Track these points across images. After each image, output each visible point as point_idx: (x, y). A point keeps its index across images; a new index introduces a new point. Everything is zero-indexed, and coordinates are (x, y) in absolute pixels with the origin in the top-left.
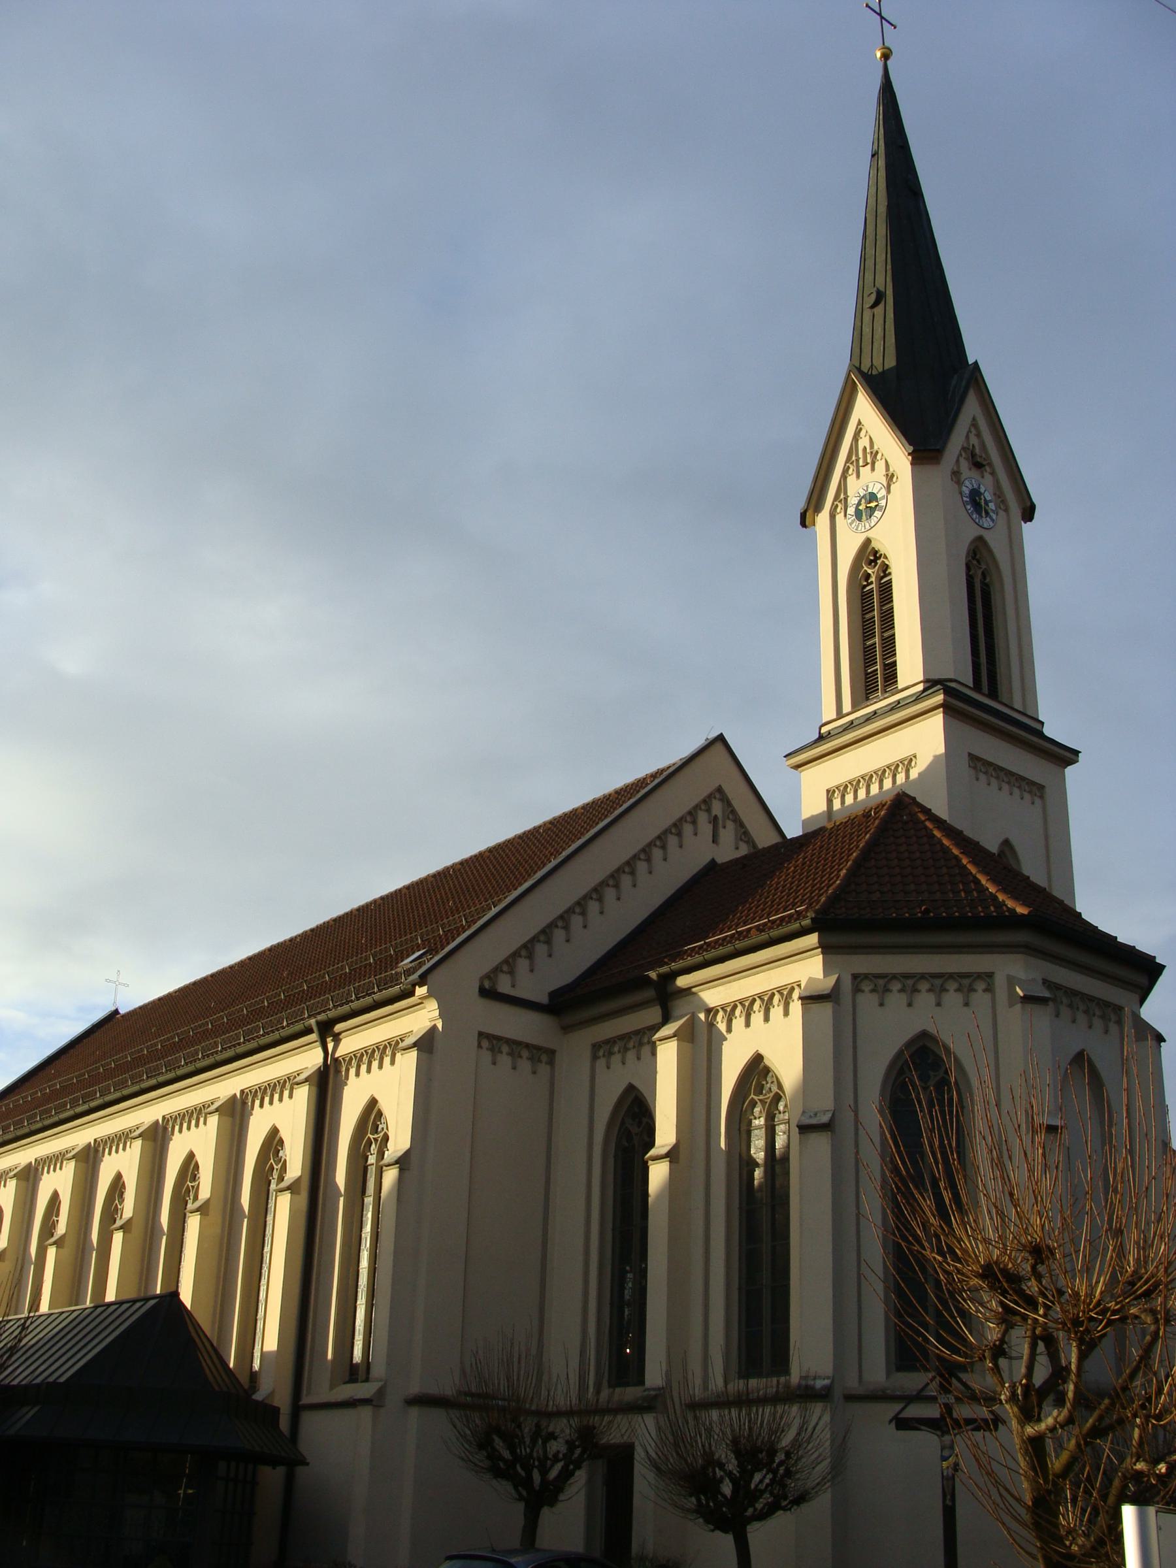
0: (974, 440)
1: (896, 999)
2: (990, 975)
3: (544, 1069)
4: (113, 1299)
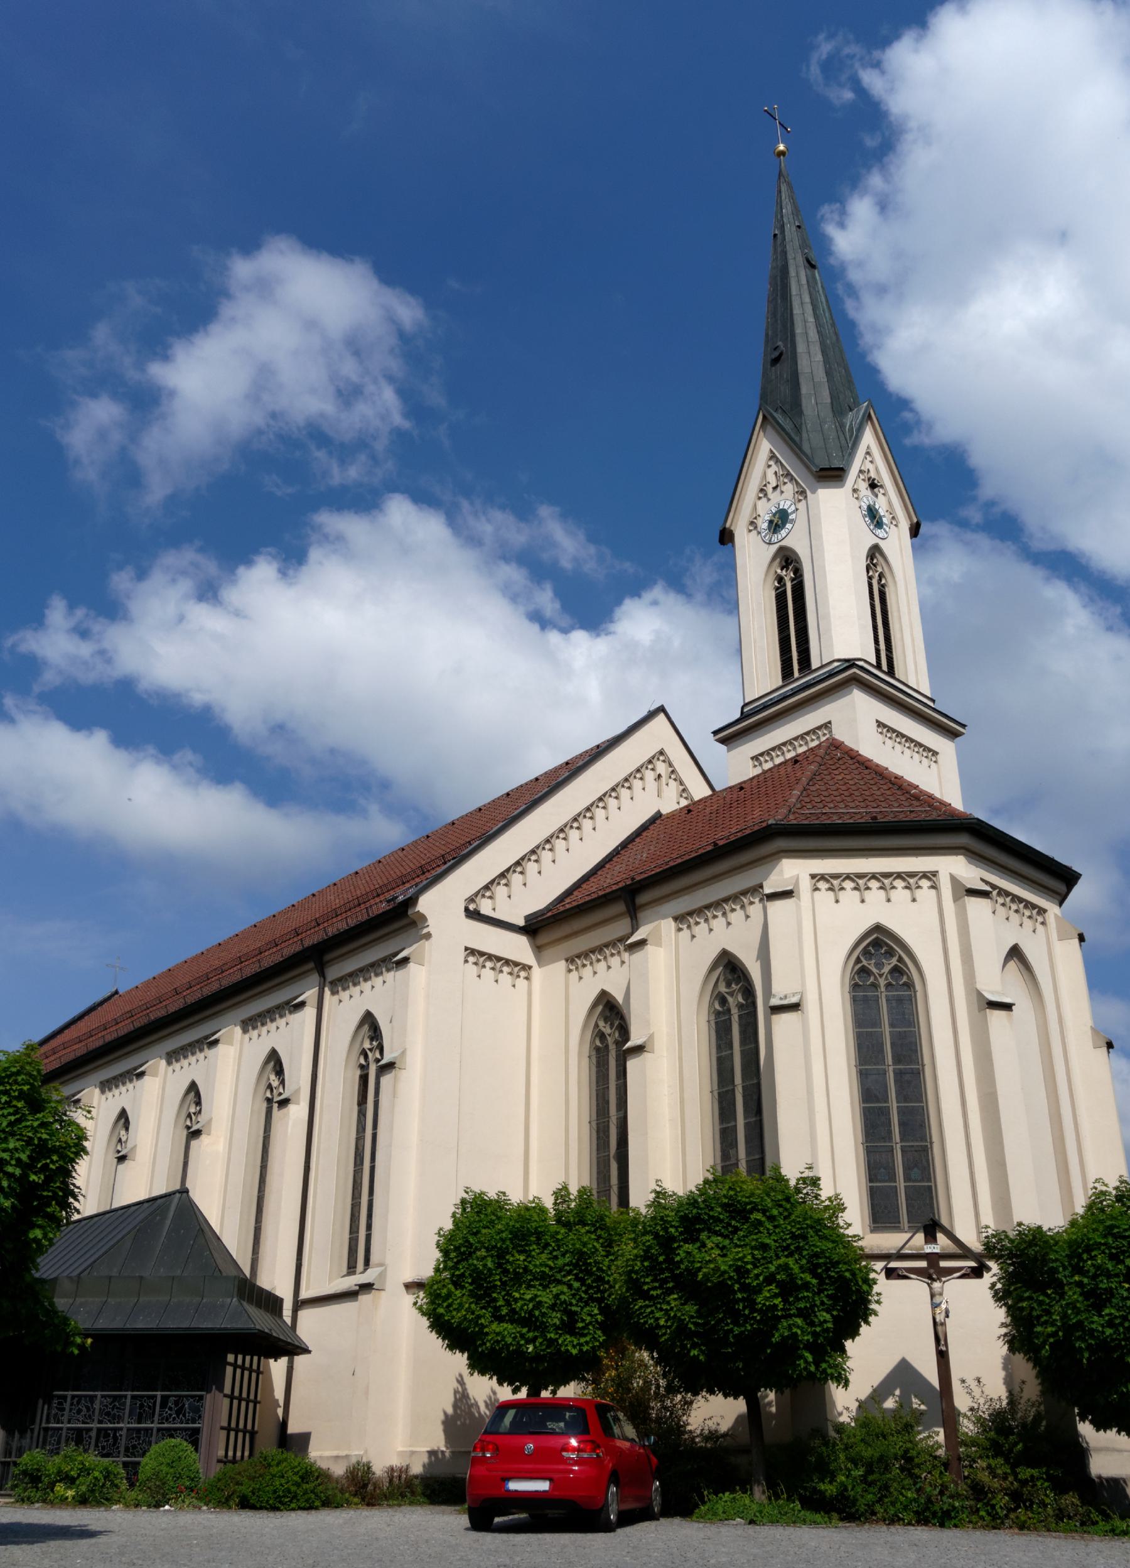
0: (871, 467)
2: (935, 874)
3: (521, 983)
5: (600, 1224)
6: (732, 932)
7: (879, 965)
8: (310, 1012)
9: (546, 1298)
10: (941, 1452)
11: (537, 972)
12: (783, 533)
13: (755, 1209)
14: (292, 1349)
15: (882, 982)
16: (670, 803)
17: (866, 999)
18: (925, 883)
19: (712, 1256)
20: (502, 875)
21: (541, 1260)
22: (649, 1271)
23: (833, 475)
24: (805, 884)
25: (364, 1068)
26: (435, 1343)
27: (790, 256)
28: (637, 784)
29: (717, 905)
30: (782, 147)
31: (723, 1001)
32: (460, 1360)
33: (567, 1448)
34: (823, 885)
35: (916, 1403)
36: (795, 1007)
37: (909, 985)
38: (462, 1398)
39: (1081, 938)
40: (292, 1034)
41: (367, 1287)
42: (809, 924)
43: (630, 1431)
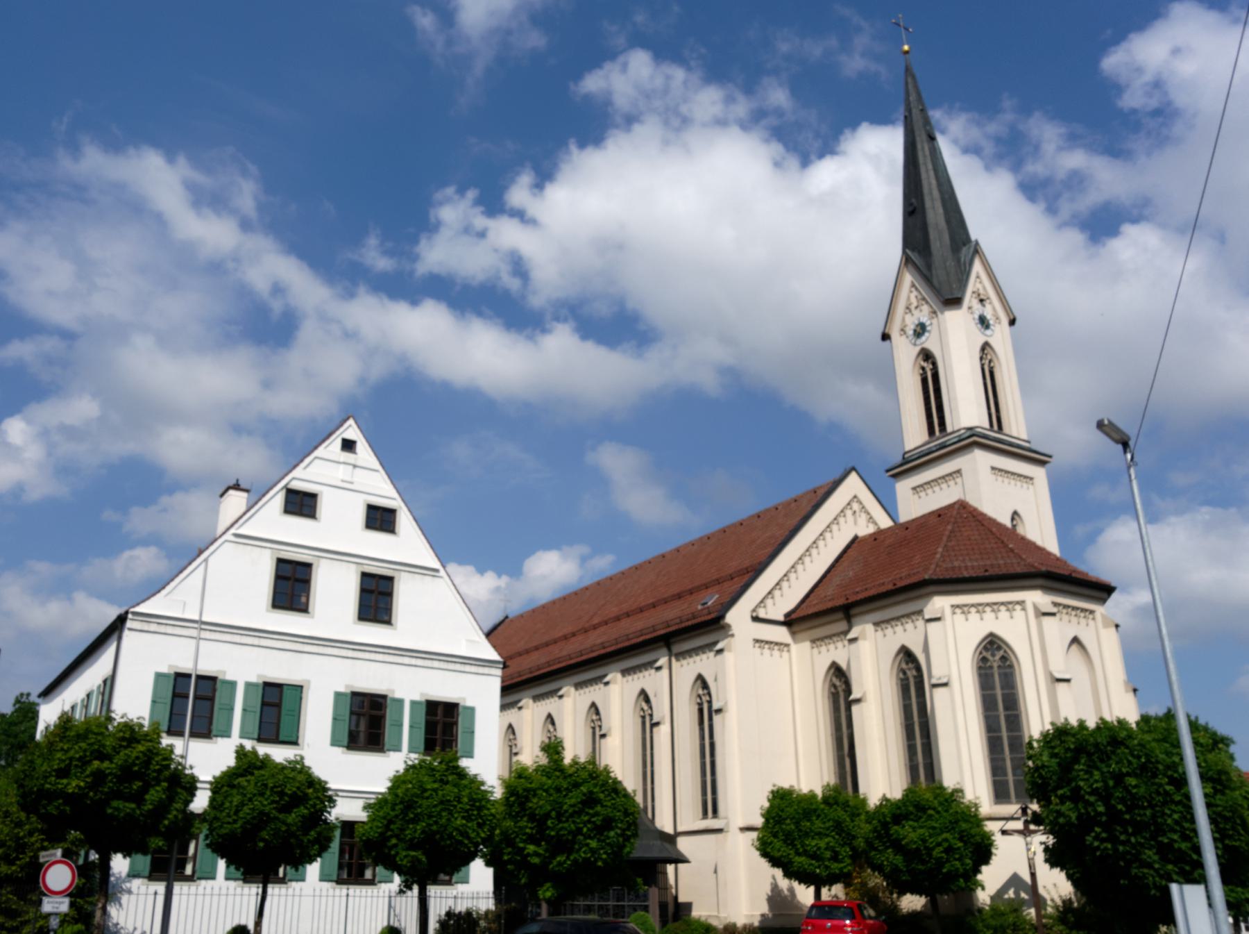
0: (979, 286)
1: (974, 616)
3: (785, 654)
4: (896, 792)
5: (846, 805)
6: (908, 634)
7: (993, 655)
8: (665, 672)
9: (822, 844)
10: (1034, 922)
11: (794, 647)
12: (923, 338)
13: (930, 808)
14: (680, 859)
15: (995, 665)
16: (865, 530)
17: (986, 675)
18: (1018, 607)
19: (910, 833)
20: (770, 593)
21: (818, 825)
22: (877, 838)
23: (953, 302)
24: (948, 611)
25: (700, 705)
26: (764, 864)
27: (917, 133)
28: (841, 520)
29: (898, 619)
30: (906, 48)
31: (905, 673)
32: (778, 873)
33: (846, 926)
34: (958, 611)
35: (1023, 895)
36: (945, 685)
37: (1011, 666)
38: (775, 887)
39: (1117, 626)
40: (655, 681)
41: (719, 831)
42: (952, 632)
43: (872, 913)
